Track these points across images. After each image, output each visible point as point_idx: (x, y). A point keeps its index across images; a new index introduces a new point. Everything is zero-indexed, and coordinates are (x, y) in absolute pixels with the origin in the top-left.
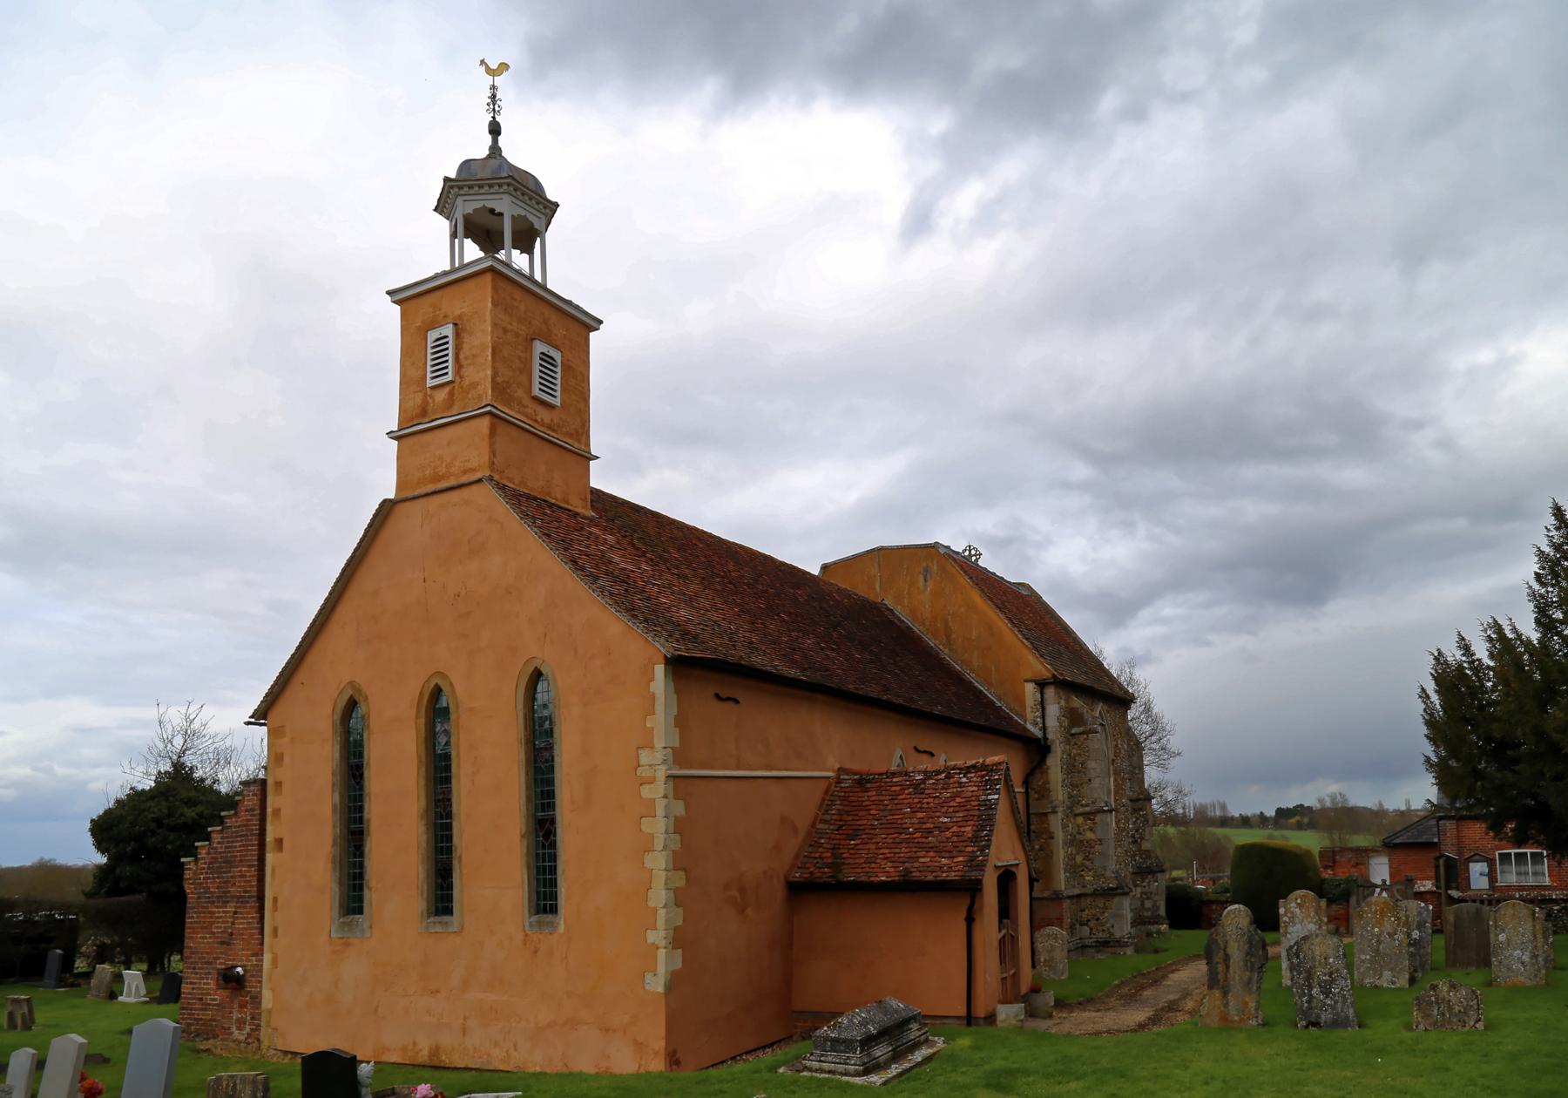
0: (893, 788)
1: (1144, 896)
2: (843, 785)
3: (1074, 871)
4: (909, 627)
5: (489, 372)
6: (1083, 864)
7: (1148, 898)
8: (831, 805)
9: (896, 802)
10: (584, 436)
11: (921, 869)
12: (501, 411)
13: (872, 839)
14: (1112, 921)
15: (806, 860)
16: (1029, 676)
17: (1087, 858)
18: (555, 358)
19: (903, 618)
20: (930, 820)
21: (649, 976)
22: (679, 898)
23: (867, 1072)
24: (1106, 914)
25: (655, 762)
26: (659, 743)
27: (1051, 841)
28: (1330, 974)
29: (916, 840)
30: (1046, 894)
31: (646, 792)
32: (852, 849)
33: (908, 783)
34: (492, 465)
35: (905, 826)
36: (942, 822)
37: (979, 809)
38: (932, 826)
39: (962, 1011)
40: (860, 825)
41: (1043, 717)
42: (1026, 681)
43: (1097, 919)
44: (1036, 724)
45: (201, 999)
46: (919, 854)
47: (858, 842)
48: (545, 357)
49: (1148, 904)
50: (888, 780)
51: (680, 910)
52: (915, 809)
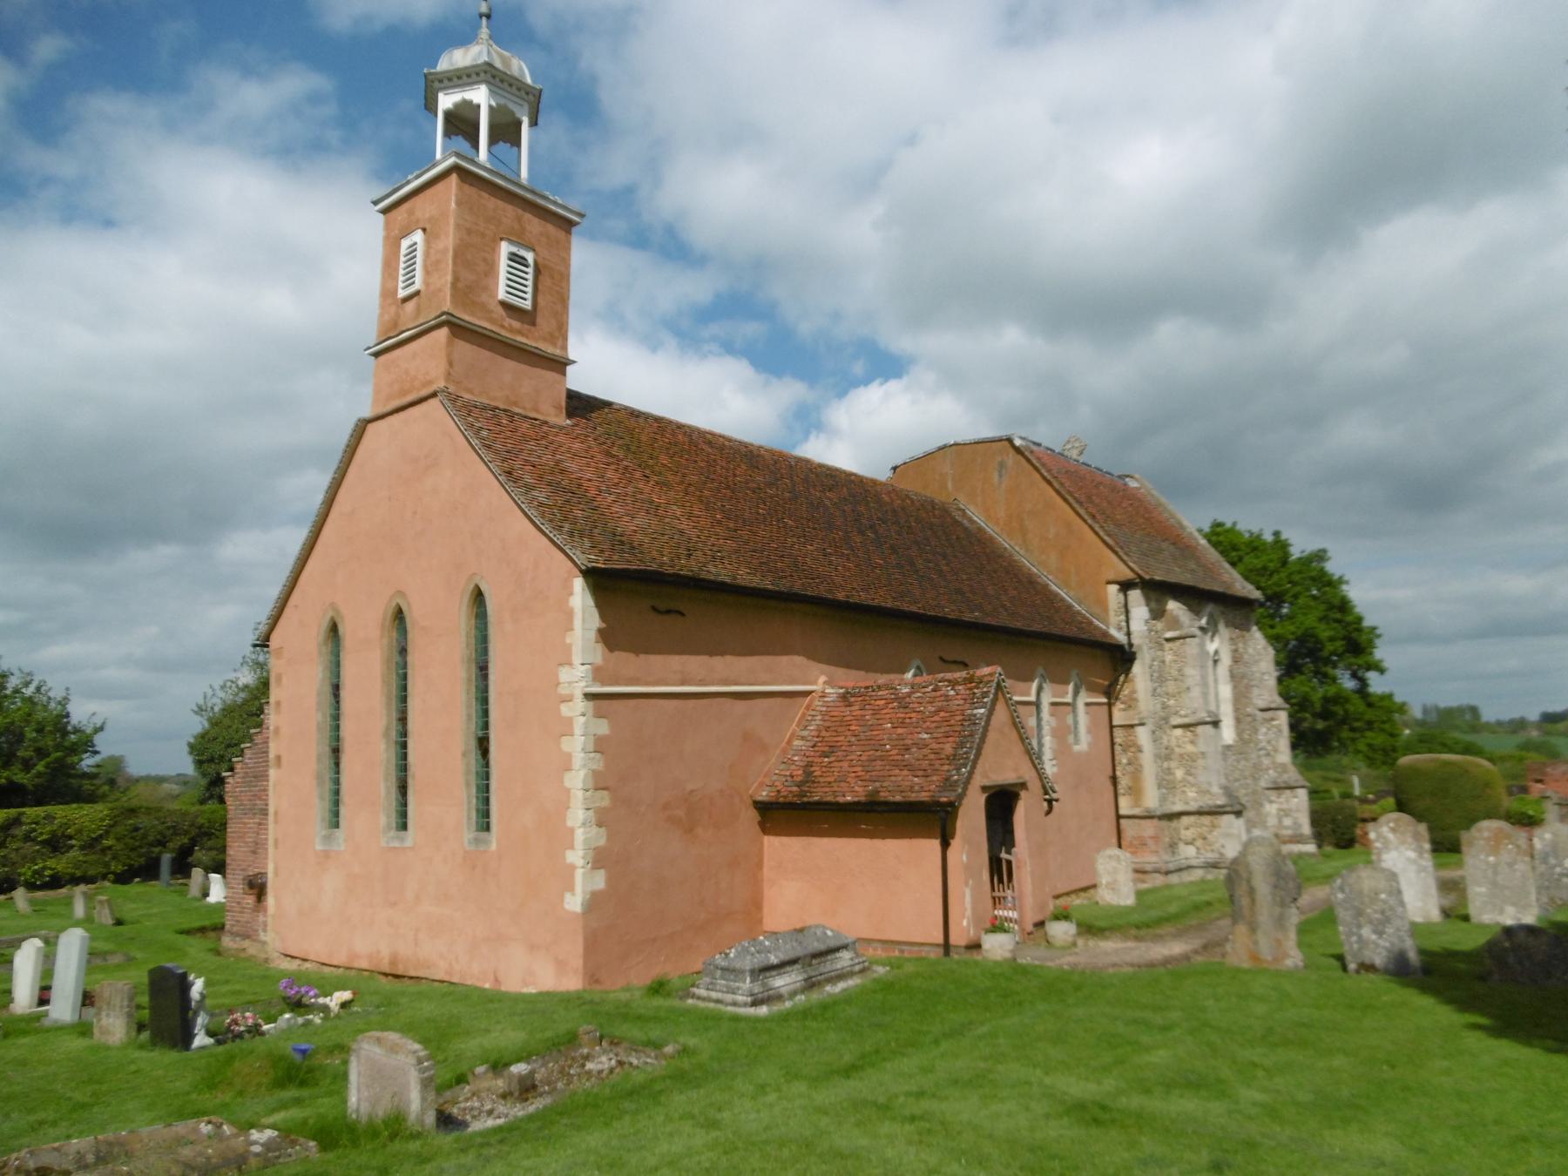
0: (878, 702)
1: (1282, 813)
2: (826, 699)
3: (1167, 784)
4: (980, 529)
5: (449, 278)
6: (1184, 780)
7: (1287, 815)
8: (812, 720)
9: (878, 716)
10: (561, 339)
11: (890, 789)
12: (458, 318)
13: (847, 756)
14: (1222, 841)
15: (775, 778)
16: (1111, 577)
17: (1188, 773)
18: (526, 257)
19: (975, 519)
20: (910, 736)
21: (568, 896)
22: (602, 819)
23: (754, 1004)
24: (1215, 833)
25: (576, 678)
26: (577, 659)
27: (1139, 755)
28: (1383, 912)
29: (891, 758)
30: (1136, 811)
31: (565, 710)
32: (825, 767)
33: (893, 696)
34: (448, 376)
35: (881, 742)
36: (922, 739)
37: (962, 725)
38: (910, 742)
39: (940, 940)
40: (837, 742)
41: (1127, 621)
42: (1109, 583)
43: (1205, 839)
44: (1119, 629)
45: (239, 903)
46: (891, 773)
47: (832, 759)
48: (513, 257)
49: (1287, 822)
50: (874, 693)
51: (603, 830)
52: (895, 725)
